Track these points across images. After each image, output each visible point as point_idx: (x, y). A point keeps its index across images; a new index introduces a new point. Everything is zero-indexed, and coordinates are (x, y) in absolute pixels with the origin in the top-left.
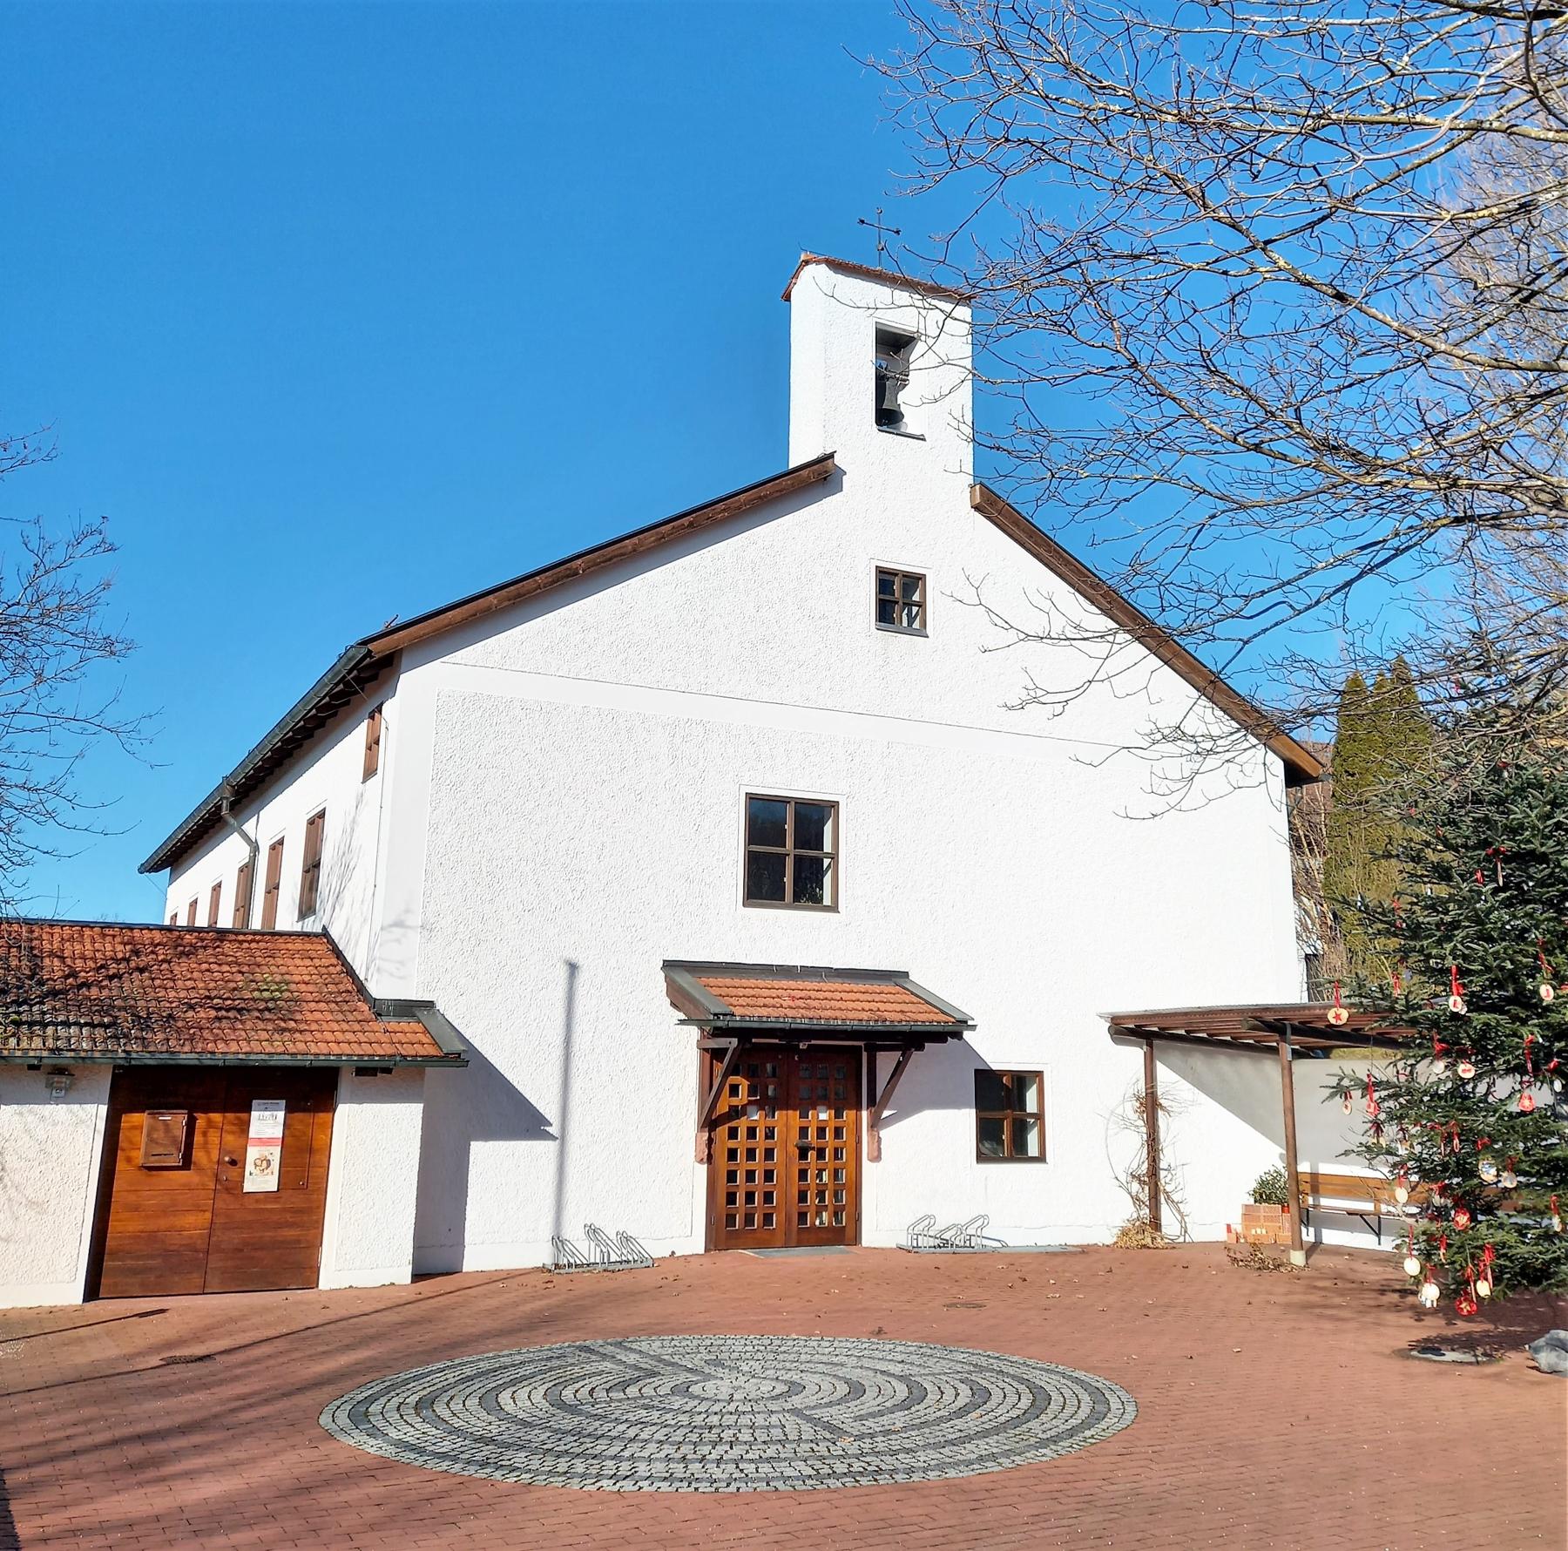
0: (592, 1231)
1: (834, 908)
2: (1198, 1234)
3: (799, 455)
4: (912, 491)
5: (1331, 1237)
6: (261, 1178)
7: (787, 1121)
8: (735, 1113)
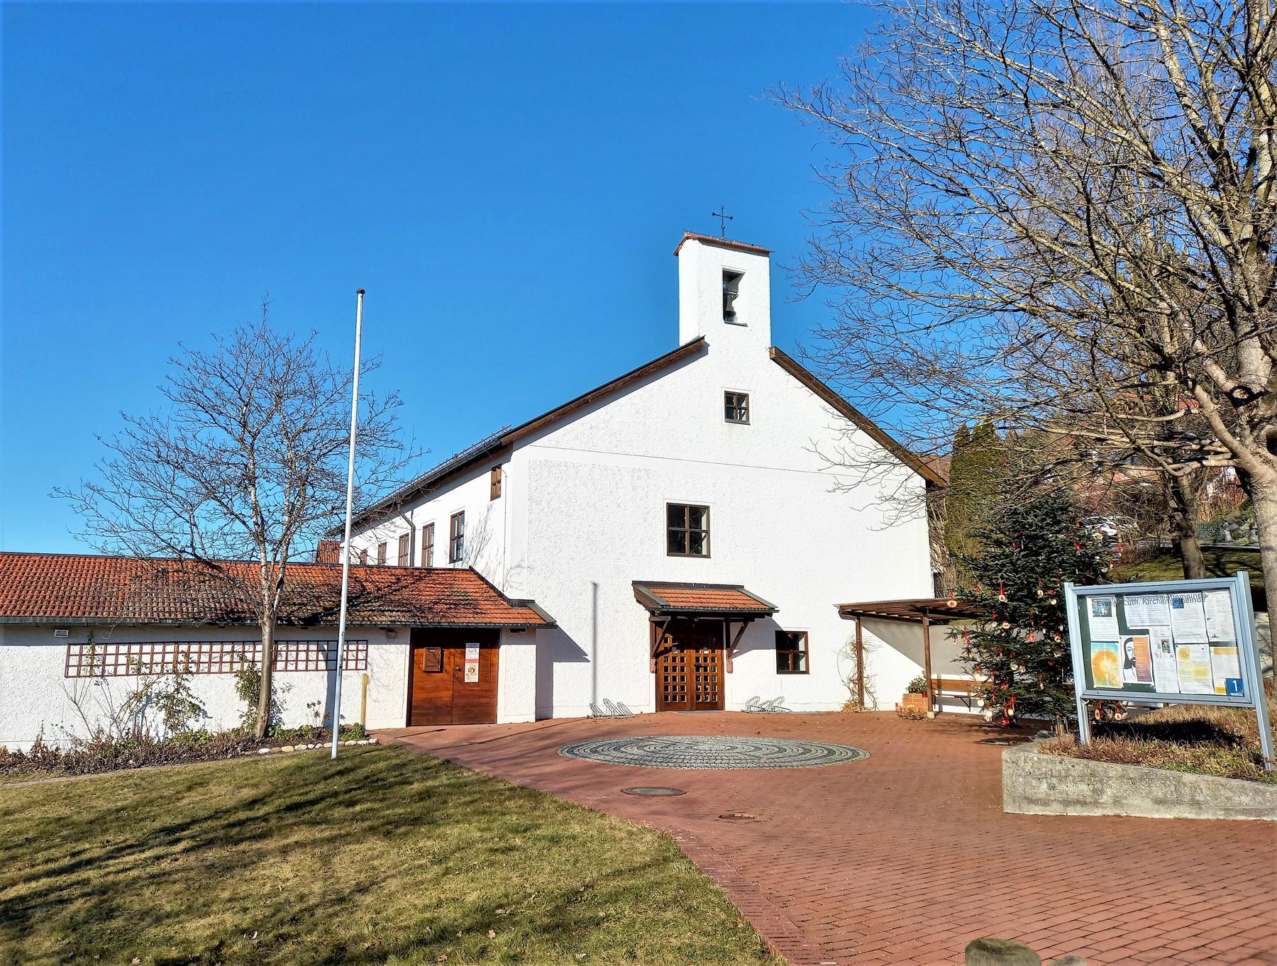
0: (606, 702)
1: (708, 556)
2: (881, 708)
3: (685, 338)
4: (741, 352)
5: (946, 709)
6: (472, 677)
7: (690, 654)
8: (667, 650)
